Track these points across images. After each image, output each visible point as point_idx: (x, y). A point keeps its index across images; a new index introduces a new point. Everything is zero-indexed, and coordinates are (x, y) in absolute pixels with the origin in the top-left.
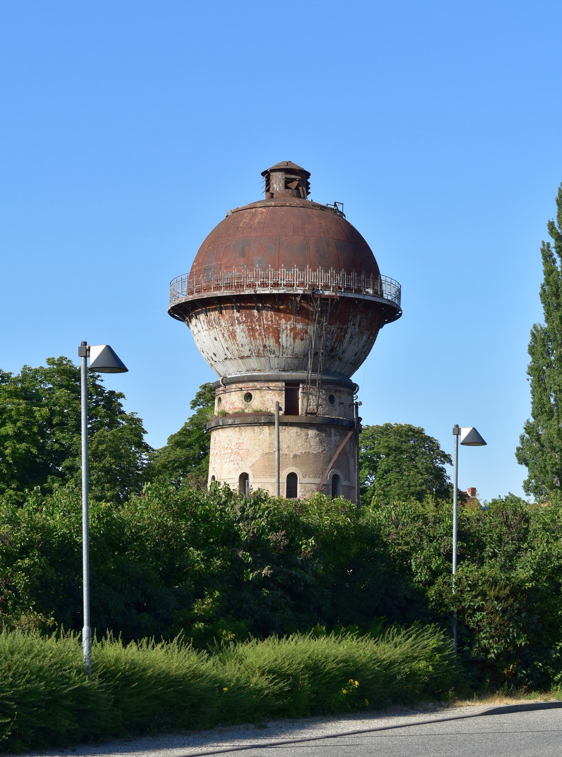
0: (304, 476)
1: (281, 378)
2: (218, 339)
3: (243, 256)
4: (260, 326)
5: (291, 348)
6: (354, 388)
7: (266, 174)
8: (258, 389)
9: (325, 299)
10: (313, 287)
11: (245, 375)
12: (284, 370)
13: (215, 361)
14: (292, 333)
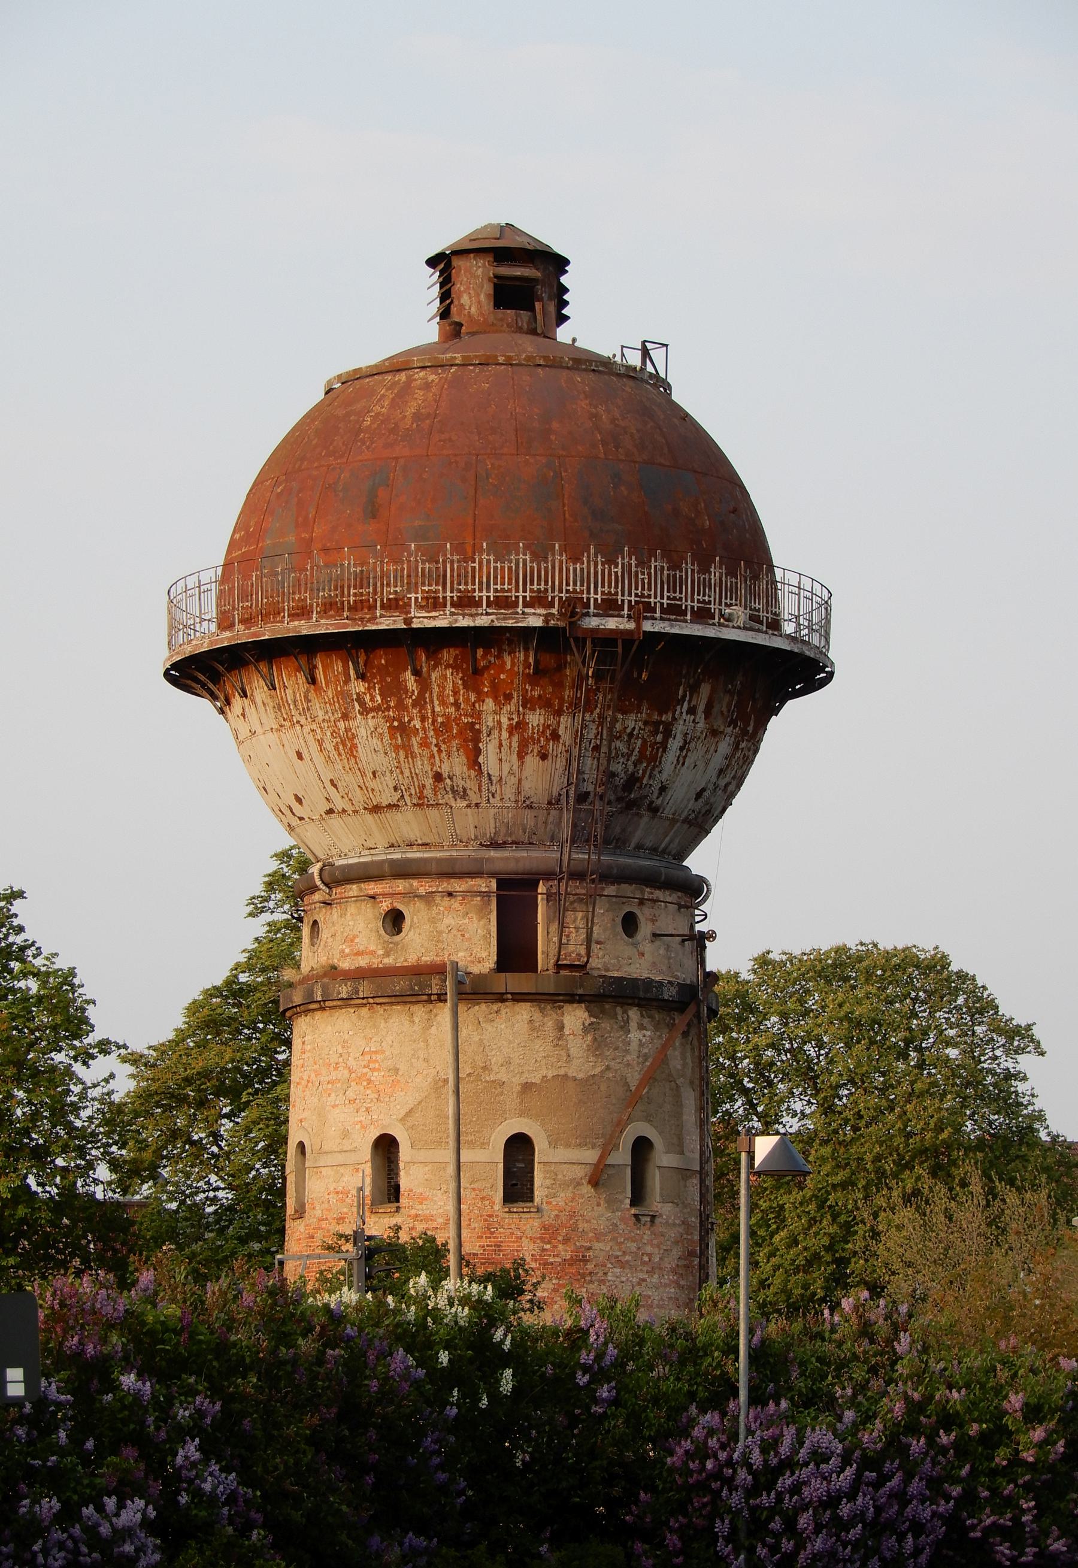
0: (553, 1143)
1: (486, 867)
2: (305, 755)
3: (374, 517)
4: (423, 719)
5: (514, 780)
6: (694, 890)
7: (441, 262)
8: (420, 897)
9: (606, 640)
10: (573, 607)
11: (384, 857)
12: (494, 845)
13: (301, 819)
14: (515, 738)
